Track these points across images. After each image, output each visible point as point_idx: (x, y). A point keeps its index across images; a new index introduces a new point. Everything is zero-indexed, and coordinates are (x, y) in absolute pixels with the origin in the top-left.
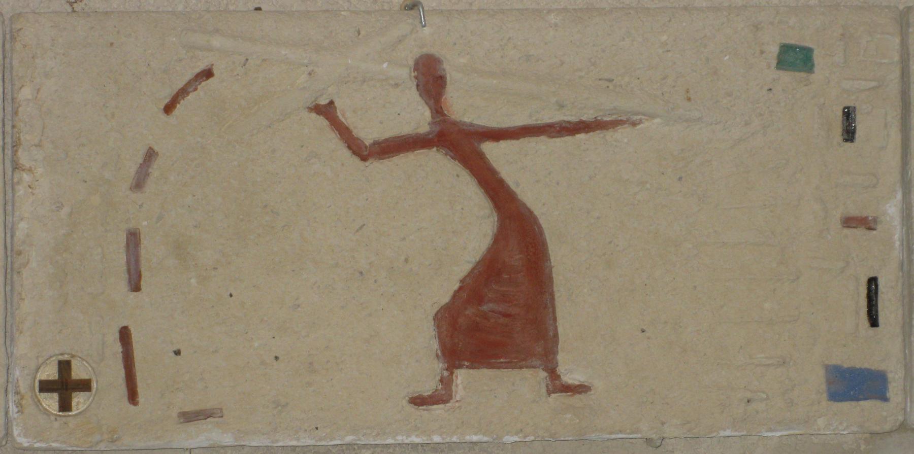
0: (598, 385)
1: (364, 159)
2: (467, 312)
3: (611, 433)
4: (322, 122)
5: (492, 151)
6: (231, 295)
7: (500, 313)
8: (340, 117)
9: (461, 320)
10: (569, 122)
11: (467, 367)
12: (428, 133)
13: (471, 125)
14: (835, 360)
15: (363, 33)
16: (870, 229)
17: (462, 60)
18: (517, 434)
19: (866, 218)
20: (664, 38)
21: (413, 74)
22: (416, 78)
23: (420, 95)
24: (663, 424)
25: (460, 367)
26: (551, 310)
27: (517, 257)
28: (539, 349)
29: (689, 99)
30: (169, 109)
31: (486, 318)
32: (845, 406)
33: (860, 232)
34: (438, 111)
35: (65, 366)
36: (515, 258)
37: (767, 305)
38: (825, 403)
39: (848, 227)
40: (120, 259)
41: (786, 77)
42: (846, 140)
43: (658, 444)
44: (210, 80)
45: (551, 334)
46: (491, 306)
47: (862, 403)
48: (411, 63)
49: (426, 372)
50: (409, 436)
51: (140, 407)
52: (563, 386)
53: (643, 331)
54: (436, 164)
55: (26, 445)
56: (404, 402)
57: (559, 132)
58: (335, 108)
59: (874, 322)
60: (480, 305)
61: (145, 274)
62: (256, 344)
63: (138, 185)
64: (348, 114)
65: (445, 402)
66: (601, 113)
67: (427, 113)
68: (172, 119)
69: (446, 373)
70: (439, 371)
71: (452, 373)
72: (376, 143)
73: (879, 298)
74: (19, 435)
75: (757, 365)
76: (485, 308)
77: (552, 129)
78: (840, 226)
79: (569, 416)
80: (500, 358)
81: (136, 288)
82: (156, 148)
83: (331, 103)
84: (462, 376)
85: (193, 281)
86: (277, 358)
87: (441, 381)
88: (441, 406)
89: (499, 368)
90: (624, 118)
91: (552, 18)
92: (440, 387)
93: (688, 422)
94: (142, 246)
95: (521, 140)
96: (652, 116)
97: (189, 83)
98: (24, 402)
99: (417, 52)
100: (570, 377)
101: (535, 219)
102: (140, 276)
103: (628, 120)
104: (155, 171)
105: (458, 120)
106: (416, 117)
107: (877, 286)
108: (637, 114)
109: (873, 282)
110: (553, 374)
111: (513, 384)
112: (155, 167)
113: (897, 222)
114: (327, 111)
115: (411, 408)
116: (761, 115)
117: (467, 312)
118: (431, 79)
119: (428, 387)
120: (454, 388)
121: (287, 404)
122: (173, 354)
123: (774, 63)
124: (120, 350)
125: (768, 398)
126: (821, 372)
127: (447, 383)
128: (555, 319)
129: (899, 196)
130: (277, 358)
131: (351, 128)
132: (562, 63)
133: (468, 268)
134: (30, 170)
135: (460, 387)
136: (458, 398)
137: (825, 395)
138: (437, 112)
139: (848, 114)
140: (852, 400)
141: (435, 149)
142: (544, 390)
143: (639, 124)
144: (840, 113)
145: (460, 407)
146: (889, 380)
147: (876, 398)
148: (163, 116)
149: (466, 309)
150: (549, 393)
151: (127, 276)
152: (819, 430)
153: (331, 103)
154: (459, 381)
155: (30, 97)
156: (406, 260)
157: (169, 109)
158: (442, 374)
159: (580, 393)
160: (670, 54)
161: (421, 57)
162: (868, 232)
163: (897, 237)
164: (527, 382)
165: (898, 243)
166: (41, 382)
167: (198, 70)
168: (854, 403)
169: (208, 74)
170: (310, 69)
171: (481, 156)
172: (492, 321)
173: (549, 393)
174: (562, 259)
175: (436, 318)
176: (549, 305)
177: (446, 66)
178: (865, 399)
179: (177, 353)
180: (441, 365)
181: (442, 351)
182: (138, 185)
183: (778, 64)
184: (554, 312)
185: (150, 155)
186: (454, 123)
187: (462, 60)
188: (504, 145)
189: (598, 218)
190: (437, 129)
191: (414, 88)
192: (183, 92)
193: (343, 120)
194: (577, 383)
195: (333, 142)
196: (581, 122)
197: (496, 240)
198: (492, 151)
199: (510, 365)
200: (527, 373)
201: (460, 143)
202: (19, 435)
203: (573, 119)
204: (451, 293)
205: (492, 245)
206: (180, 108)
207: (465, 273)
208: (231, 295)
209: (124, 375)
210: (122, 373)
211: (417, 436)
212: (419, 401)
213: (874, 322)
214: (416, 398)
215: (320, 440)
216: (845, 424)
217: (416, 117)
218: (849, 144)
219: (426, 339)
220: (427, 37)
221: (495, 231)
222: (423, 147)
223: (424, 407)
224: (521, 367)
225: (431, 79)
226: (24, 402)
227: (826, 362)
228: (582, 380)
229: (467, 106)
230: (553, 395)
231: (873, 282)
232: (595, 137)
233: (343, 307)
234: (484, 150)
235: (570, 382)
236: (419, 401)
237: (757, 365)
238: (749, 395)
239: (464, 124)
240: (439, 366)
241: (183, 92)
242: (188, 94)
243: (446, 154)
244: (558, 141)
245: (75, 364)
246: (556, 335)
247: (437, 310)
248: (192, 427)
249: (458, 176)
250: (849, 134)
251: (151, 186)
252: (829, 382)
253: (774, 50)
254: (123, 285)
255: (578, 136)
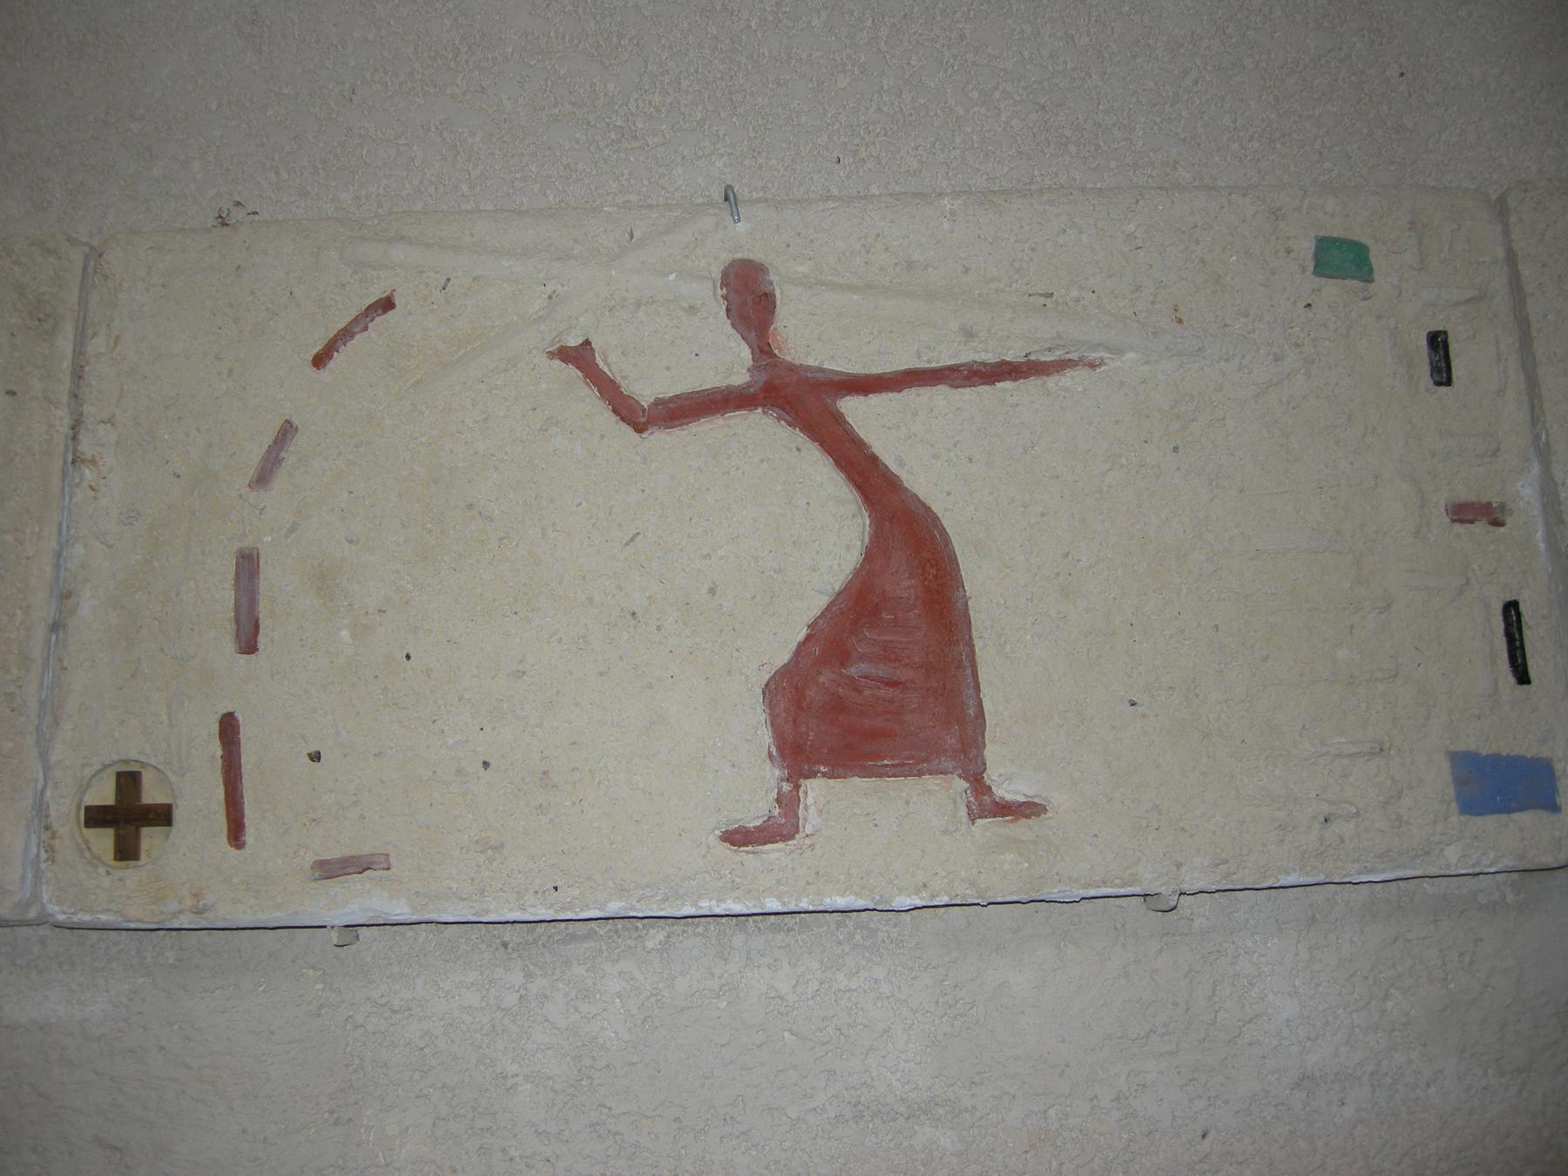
0: (1059, 799)
1: (640, 429)
2: (822, 679)
3: (1088, 886)
4: (572, 372)
5: (857, 411)
6: (408, 657)
7: (881, 680)
8: (599, 361)
9: (811, 693)
10: (984, 364)
11: (824, 775)
12: (749, 385)
13: (821, 370)
14: (1468, 743)
15: (637, 234)
16: (1497, 523)
17: (800, 269)
18: (917, 891)
19: (1489, 504)
20: (1132, 227)
21: (719, 292)
22: (725, 298)
23: (733, 325)
24: (1179, 866)
25: (812, 775)
26: (969, 671)
27: (907, 583)
28: (951, 741)
29: (1180, 321)
30: (320, 361)
31: (856, 690)
32: (1489, 822)
33: (1480, 528)
34: (763, 351)
35: (129, 781)
36: (902, 584)
37: (1342, 654)
38: (1455, 819)
39: (1462, 521)
40: (226, 596)
41: (1332, 289)
42: (1438, 384)
43: (1173, 904)
44: (390, 314)
45: (971, 712)
46: (864, 667)
47: (1515, 816)
48: (717, 274)
49: (754, 786)
50: (720, 901)
51: (247, 851)
52: (997, 804)
53: (1133, 704)
54: (761, 431)
55: (61, 917)
56: (713, 840)
57: (967, 378)
58: (593, 350)
59: (1523, 677)
60: (843, 665)
61: (264, 623)
62: (451, 741)
63: (263, 478)
64: (612, 358)
65: (787, 838)
66: (1036, 348)
67: (746, 353)
68: (325, 375)
69: (786, 787)
70: (774, 783)
71: (797, 787)
72: (658, 402)
73: (1526, 632)
74: (50, 901)
75: (1338, 756)
76: (853, 671)
77: (956, 374)
78: (1447, 520)
79: (1009, 857)
80: (884, 758)
81: (249, 645)
82: (296, 421)
83: (587, 343)
84: (815, 790)
85: (345, 634)
86: (486, 764)
87: (778, 801)
88: (780, 845)
89: (881, 776)
90: (1074, 356)
91: (946, 202)
92: (776, 812)
93: (1225, 862)
94: (262, 577)
95: (905, 392)
96: (1119, 352)
97: (356, 320)
98: (57, 843)
99: (726, 257)
100: (1005, 791)
101: (935, 519)
102: (257, 627)
103: (1081, 359)
104: (290, 456)
105: (797, 362)
106: (730, 361)
107: (1519, 615)
108: (1095, 347)
109: (1511, 610)
110: (978, 784)
111: (907, 803)
112: (292, 448)
113: (1536, 510)
114: (580, 357)
115: (724, 850)
116: (1298, 346)
117: (822, 679)
118: (749, 299)
119: (757, 809)
120: (801, 812)
121: (503, 845)
122: (307, 760)
123: (1311, 265)
124: (220, 752)
125: (1358, 814)
126: (1446, 766)
127: (789, 803)
128: (977, 687)
129: (1536, 469)
130: (486, 764)
131: (618, 380)
132: (967, 271)
133: (820, 603)
134: (93, 461)
135: (812, 810)
136: (809, 829)
137: (1454, 805)
138: (762, 351)
139: (1438, 343)
140: (1499, 812)
141: (760, 410)
142: (963, 812)
143: (1100, 365)
144: (1424, 342)
145: (812, 847)
146: (1558, 774)
147: (1535, 807)
148: (311, 371)
149: (819, 673)
150: (973, 817)
151: (234, 627)
152: (1448, 866)
153: (587, 343)
154: (810, 801)
155: (102, 350)
156: (712, 591)
157: (320, 361)
158: (780, 789)
159: (1028, 817)
160: (1141, 253)
161: (734, 263)
162: (1493, 528)
163: (1539, 535)
164: (934, 798)
165: (1542, 546)
166: (88, 809)
167: (373, 299)
168: (1504, 817)
169: (387, 304)
170: (549, 289)
171: (839, 419)
172: (867, 692)
173: (973, 817)
174: (984, 585)
175: (768, 690)
176: (966, 663)
177: (773, 277)
178: (1522, 809)
179: (316, 757)
180: (777, 772)
181: (778, 748)
182: (263, 478)
183: (1316, 267)
184: (975, 675)
185: (287, 431)
186: (792, 368)
187: (800, 269)
188: (874, 400)
189: (1043, 515)
190: (762, 378)
191: (723, 313)
192: (346, 334)
193: (606, 370)
194: (1022, 799)
195: (589, 402)
196: (1004, 363)
197: (869, 557)
198: (857, 411)
199: (901, 770)
200: (931, 782)
201: (804, 401)
202: (50, 901)
203: (990, 358)
204: (793, 646)
205: (862, 566)
206: (338, 360)
207: (816, 612)
208: (408, 657)
209: (222, 796)
210: (220, 793)
211: (737, 900)
212: (738, 838)
213: (1523, 677)
214: (736, 831)
215: (563, 909)
216: (1492, 855)
217: (730, 361)
218: (1443, 389)
219: (752, 730)
220: (745, 237)
221: (867, 540)
222: (739, 407)
223: (750, 848)
224: (920, 774)
225: (749, 299)
226: (57, 843)
227: (1451, 748)
228: (1030, 793)
229: (810, 337)
230: (979, 821)
231: (1511, 610)
232: (1032, 384)
233: (601, 674)
234: (843, 410)
235: (1009, 797)
236: (738, 838)
237: (1338, 756)
238: (1326, 808)
239: (808, 368)
240: (773, 774)
241: (346, 334)
242: (352, 337)
243: (779, 419)
244: (966, 393)
245: (147, 778)
246: (981, 713)
247: (767, 677)
248: (335, 887)
249: (798, 450)
250: (1442, 373)
251: (280, 481)
252: (1459, 782)
253: (1307, 248)
254: (228, 645)
255: (999, 385)
